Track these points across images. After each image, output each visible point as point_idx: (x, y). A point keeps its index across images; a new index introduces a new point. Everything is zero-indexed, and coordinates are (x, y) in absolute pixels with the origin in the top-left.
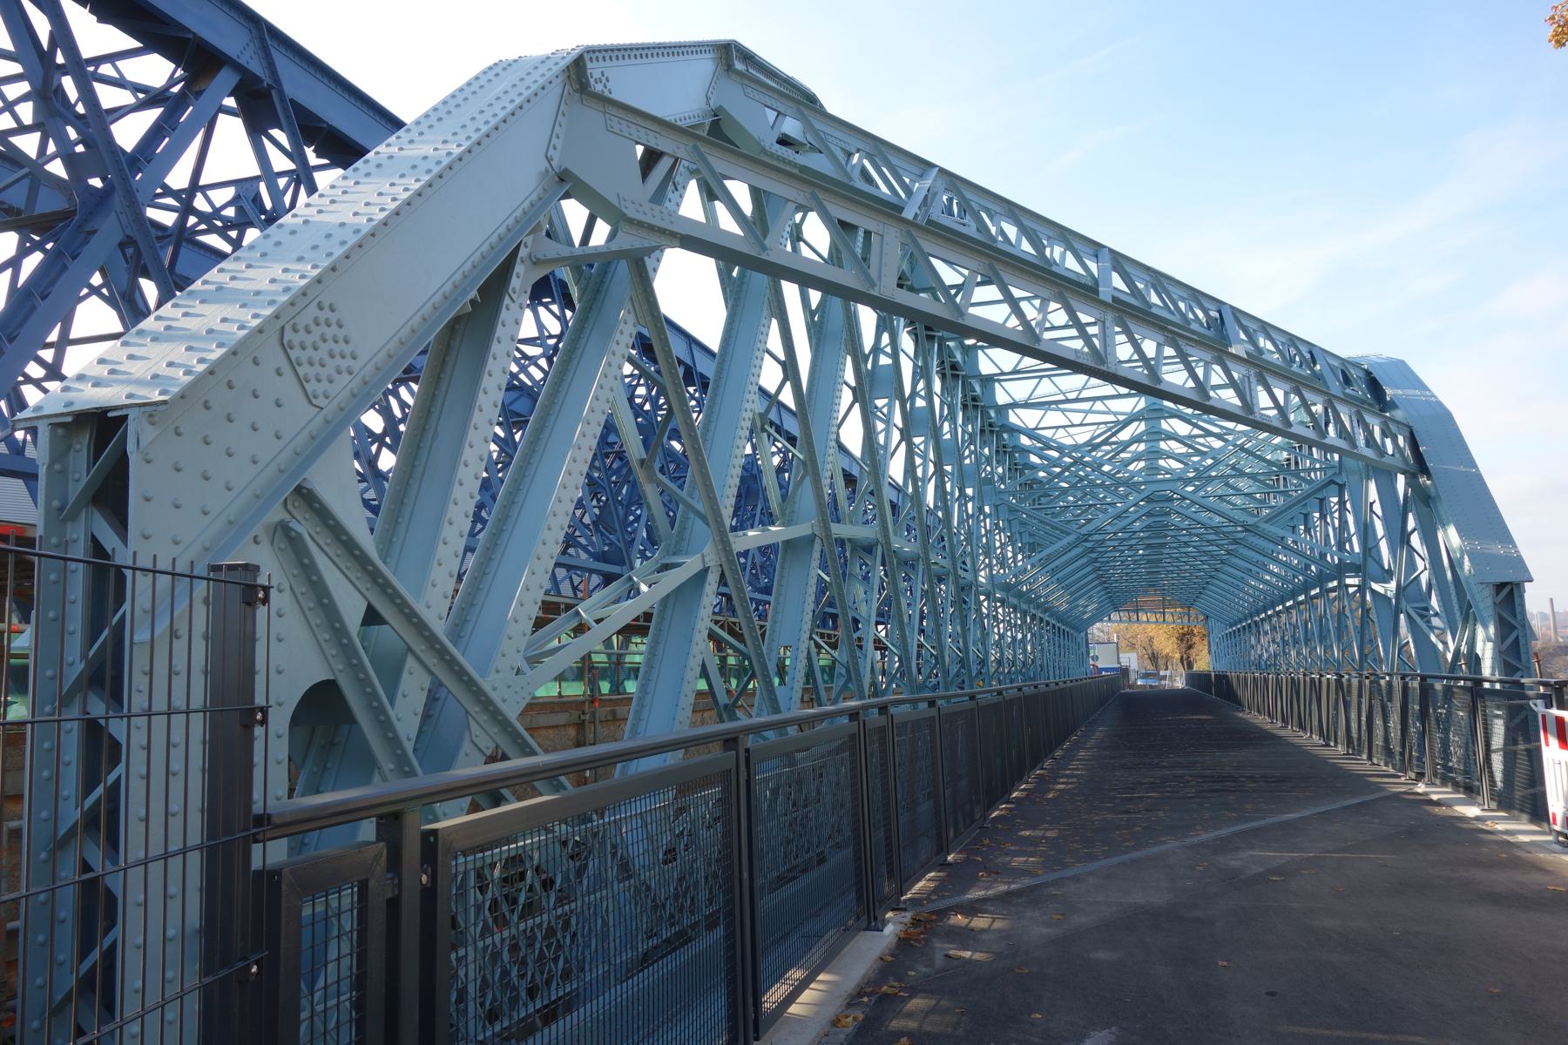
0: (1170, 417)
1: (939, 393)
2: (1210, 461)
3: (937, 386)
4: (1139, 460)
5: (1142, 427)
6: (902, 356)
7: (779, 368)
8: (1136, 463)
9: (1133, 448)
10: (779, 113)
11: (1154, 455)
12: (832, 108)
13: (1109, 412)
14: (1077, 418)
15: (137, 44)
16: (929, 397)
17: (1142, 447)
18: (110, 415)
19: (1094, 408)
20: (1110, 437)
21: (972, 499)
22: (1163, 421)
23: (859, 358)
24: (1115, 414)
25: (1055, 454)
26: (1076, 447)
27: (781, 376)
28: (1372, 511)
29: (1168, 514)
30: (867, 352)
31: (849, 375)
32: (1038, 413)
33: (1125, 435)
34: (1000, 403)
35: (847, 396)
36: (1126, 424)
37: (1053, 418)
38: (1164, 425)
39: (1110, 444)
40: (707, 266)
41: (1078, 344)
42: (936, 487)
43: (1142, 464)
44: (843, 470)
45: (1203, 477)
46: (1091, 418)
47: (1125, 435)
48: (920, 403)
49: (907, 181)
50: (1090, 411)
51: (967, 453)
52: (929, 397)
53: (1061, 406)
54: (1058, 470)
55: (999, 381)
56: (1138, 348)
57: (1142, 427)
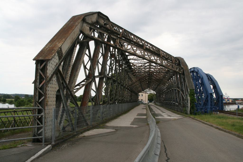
2: (158, 70)
4: (148, 69)
5: (149, 64)
9: (147, 67)
11: (150, 68)
12: (111, 20)
13: (144, 61)
14: (139, 62)
15: (107, 65)
17: (148, 67)
21: (118, 66)
23: (110, 52)
25: (136, 67)
26: (139, 66)
28: (178, 79)
29: (151, 77)
31: (109, 55)
32: (134, 61)
33: (146, 65)
34: (128, 59)
35: (109, 58)
37: (136, 62)
38: (152, 64)
39: (144, 66)
41: (141, 54)
43: (148, 69)
45: (156, 72)
47: (146, 65)
49: (119, 29)
51: (121, 62)
55: (129, 56)
57: (149, 64)
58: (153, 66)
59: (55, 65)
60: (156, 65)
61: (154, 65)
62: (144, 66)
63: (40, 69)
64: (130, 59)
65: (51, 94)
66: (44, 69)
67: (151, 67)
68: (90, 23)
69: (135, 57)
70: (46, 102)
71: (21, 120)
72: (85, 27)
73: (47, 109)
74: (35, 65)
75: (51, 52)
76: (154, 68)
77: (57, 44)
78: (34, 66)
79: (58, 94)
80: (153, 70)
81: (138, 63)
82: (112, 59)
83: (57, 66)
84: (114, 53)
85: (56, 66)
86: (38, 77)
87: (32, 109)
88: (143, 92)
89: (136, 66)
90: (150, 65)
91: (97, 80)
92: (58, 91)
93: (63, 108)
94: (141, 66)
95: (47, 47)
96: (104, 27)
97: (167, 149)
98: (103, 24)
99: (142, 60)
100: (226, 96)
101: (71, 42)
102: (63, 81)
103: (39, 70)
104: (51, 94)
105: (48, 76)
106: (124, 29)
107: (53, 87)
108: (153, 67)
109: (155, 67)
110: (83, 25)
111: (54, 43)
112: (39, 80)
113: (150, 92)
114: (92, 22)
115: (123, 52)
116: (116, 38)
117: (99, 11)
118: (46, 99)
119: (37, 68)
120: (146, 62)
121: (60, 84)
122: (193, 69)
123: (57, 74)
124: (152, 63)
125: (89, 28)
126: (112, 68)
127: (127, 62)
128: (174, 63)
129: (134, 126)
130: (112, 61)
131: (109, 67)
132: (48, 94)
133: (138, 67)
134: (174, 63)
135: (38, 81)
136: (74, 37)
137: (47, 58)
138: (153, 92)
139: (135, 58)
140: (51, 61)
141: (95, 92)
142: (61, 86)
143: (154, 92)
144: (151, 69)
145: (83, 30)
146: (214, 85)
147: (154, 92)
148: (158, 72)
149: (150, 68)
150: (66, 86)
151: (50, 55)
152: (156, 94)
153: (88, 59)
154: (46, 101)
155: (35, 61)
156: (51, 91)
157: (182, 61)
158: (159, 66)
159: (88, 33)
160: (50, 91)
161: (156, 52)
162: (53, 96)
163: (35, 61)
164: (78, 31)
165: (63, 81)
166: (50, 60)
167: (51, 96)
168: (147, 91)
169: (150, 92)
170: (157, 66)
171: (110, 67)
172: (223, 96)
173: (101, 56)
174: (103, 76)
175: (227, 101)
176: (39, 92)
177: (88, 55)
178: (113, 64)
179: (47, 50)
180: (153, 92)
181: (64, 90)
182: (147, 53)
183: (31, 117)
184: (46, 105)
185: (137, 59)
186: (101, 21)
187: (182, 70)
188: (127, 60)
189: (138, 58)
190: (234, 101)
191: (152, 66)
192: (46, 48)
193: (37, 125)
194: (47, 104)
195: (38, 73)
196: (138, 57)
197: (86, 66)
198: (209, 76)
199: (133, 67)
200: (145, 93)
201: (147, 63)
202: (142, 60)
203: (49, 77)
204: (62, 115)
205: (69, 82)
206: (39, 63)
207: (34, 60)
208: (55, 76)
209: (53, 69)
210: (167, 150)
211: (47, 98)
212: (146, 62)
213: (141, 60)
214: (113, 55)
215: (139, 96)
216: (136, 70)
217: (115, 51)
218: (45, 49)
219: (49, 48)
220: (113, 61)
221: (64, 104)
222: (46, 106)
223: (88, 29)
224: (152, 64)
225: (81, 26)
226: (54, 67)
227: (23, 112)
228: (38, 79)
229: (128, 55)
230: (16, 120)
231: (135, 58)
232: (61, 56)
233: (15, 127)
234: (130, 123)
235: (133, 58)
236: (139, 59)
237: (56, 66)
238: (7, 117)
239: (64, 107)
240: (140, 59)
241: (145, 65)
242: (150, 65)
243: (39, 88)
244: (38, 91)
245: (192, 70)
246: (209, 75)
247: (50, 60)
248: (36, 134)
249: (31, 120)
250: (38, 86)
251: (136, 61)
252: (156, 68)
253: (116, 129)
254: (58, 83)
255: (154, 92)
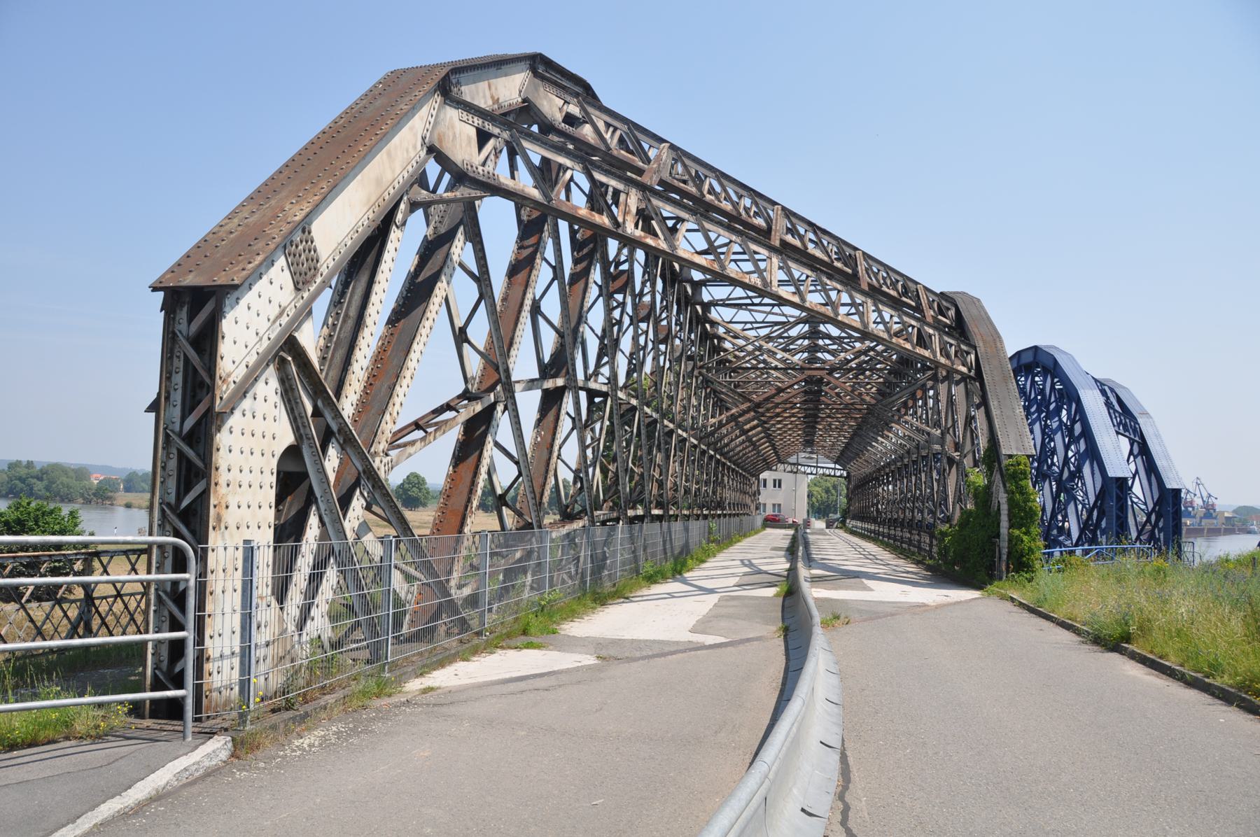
0: (827, 323)
1: (661, 291)
3: (659, 285)
6: (636, 264)
7: (550, 270)
8: (801, 354)
9: (800, 342)
10: (566, 102)
14: (760, 317)
16: (653, 292)
17: (806, 342)
18: (206, 290)
19: (773, 311)
20: (783, 333)
22: (821, 325)
24: (746, 309)
27: (551, 276)
30: (611, 260)
33: (794, 332)
35: (594, 291)
36: (796, 323)
37: (744, 315)
38: (822, 328)
39: (783, 338)
40: (510, 206)
42: (654, 359)
44: (872, 590)
46: (771, 318)
47: (794, 332)
48: (647, 299)
50: (770, 313)
52: (653, 292)
53: (749, 307)
54: (742, 354)
55: (706, 286)
56: (664, 319)
57: (807, 328)
58: (829, 337)
59: (272, 318)
60: (843, 335)
61: (835, 332)
62: (780, 336)
63: (187, 339)
64: (714, 303)
65: (246, 470)
66: (207, 340)
67: (821, 342)
68: (483, 105)
69: (739, 292)
70: (212, 511)
71: (126, 599)
72: (452, 126)
73: (220, 544)
74: (160, 317)
75: (250, 245)
76: (835, 347)
77: (287, 207)
78: (157, 320)
79: (292, 467)
80: (828, 357)
81: (751, 323)
82: (617, 301)
83: (284, 320)
84: (625, 267)
85: (274, 322)
86: (178, 379)
87: (146, 546)
88: (780, 467)
89: (746, 339)
90: (814, 334)
91: (529, 403)
92: (292, 453)
93: (320, 540)
94: (768, 338)
95: (236, 221)
96: (561, 133)
97: (855, 775)
98: (559, 117)
99: (773, 305)
100: (1199, 495)
101: (373, 200)
102: (320, 403)
103: (184, 342)
104: (246, 470)
105: (229, 375)
106: (667, 142)
107: (258, 434)
108: (828, 342)
109: (839, 345)
110: (442, 116)
111: (273, 202)
112: (180, 392)
113: (817, 467)
114: (496, 101)
115: (677, 266)
116: (620, 186)
117: (538, 52)
118: (216, 491)
119: (174, 333)
120: (793, 317)
121: (301, 417)
122: (1031, 353)
123: (282, 365)
124: (824, 323)
125: (473, 132)
126: (616, 342)
127: (701, 321)
128: (930, 320)
129: (710, 640)
130: (615, 308)
131: (597, 341)
132: (223, 469)
133: (752, 343)
134: (930, 320)
135: (177, 397)
136: (389, 176)
137: (221, 280)
138: (833, 466)
139: (740, 298)
140: (249, 298)
141: (517, 463)
142: (304, 427)
143: (838, 467)
144: (819, 355)
145: (440, 140)
146: (1137, 439)
147: (835, 469)
148: (851, 369)
149: (813, 349)
150: (339, 431)
151: (238, 262)
152: (845, 478)
153: (477, 296)
154: (213, 501)
155: (161, 295)
156: (247, 451)
157: (974, 312)
158: (857, 339)
159: (467, 157)
160: (236, 451)
161: (838, 265)
162: (255, 478)
163: (161, 295)
164: (415, 147)
165: (320, 403)
166: (236, 287)
167: (246, 478)
168: (801, 461)
169: (817, 467)
170: (850, 337)
171: (601, 339)
172: (1183, 495)
173: (553, 280)
174: (560, 382)
175: (1204, 522)
176: (181, 454)
177: (474, 268)
178: (620, 322)
179: (232, 236)
180: (833, 466)
181: (324, 448)
182: (852, 297)
183: (127, 589)
184: (212, 523)
185: (748, 301)
186: (545, 103)
187: (973, 356)
188: (699, 308)
189: (750, 298)
190: (1238, 523)
191: (822, 339)
192: (227, 228)
193: (172, 630)
194: (219, 518)
195: (178, 357)
196: (751, 294)
197: (468, 330)
198: (1112, 390)
199: (727, 345)
200: (791, 472)
201: (799, 321)
202: (773, 305)
203: (231, 380)
204: (315, 579)
205: (363, 406)
206: (182, 307)
207: (155, 289)
208: (271, 374)
209: (261, 339)
210: (851, 786)
211: (222, 489)
212: (792, 320)
213: (768, 309)
214: (617, 282)
215: (765, 486)
216: (744, 357)
217: (631, 259)
218: (222, 234)
219: (240, 228)
220: (619, 310)
221: (326, 519)
222: (214, 528)
223: (469, 138)
224: (822, 328)
225: (432, 120)
226: (263, 325)
227: (133, 558)
228: (175, 390)
229: (703, 283)
230: (98, 598)
231: (740, 298)
232: (309, 274)
233: (89, 632)
234: (692, 622)
235: (725, 297)
236: (757, 301)
237: (274, 322)
238: (113, 583)
239: (324, 536)
240: (760, 304)
241: (786, 331)
242: (814, 334)
243: (179, 435)
244: (175, 451)
245: (1027, 359)
246: (1110, 388)
247: (236, 287)
248: (161, 677)
249: (126, 607)
250: (177, 428)
251: (741, 312)
252: (843, 348)
253: (604, 653)
254: (292, 409)
255: (835, 469)
